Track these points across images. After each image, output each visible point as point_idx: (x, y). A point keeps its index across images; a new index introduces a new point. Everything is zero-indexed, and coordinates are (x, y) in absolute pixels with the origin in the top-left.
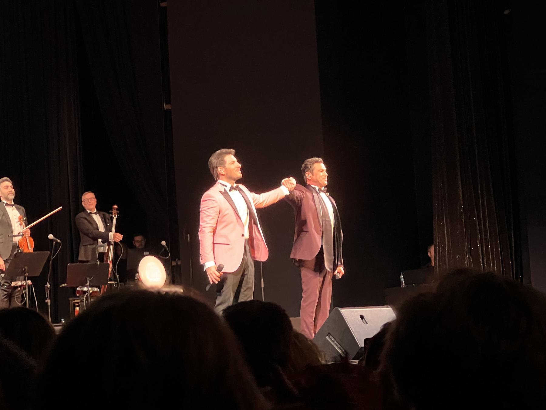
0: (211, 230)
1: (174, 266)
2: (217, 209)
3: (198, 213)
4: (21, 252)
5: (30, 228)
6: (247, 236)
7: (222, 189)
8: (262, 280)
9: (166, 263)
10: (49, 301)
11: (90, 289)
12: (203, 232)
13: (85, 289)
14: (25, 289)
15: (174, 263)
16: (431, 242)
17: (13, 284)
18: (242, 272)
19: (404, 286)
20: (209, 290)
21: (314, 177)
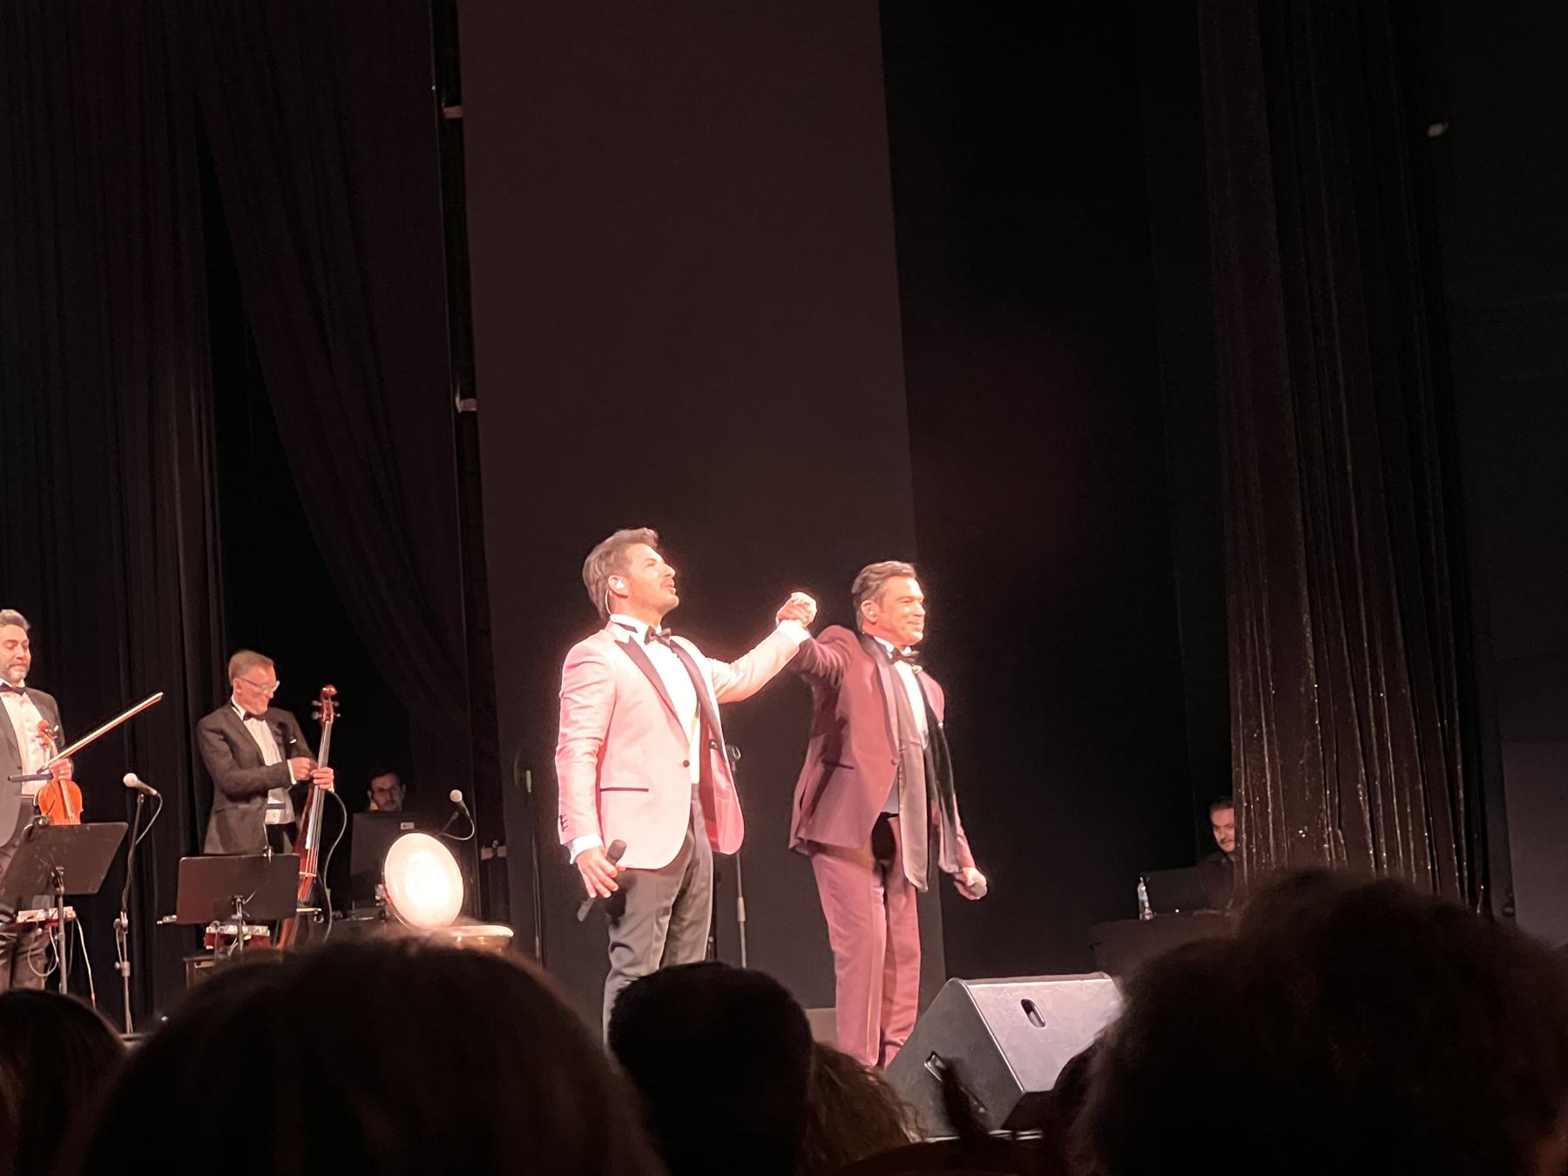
0: (590, 749)
1: (486, 861)
2: (609, 688)
3: (555, 703)
4: (45, 826)
5: (73, 757)
6: (696, 780)
7: (624, 636)
8: (741, 900)
9: (464, 855)
10: (126, 965)
11: (245, 929)
12: (568, 754)
13: (231, 929)
14: (56, 931)
15: (486, 854)
16: (1223, 794)
17: (22, 917)
18: (685, 863)
19: (1148, 914)
20: (587, 918)
21: (885, 616)
